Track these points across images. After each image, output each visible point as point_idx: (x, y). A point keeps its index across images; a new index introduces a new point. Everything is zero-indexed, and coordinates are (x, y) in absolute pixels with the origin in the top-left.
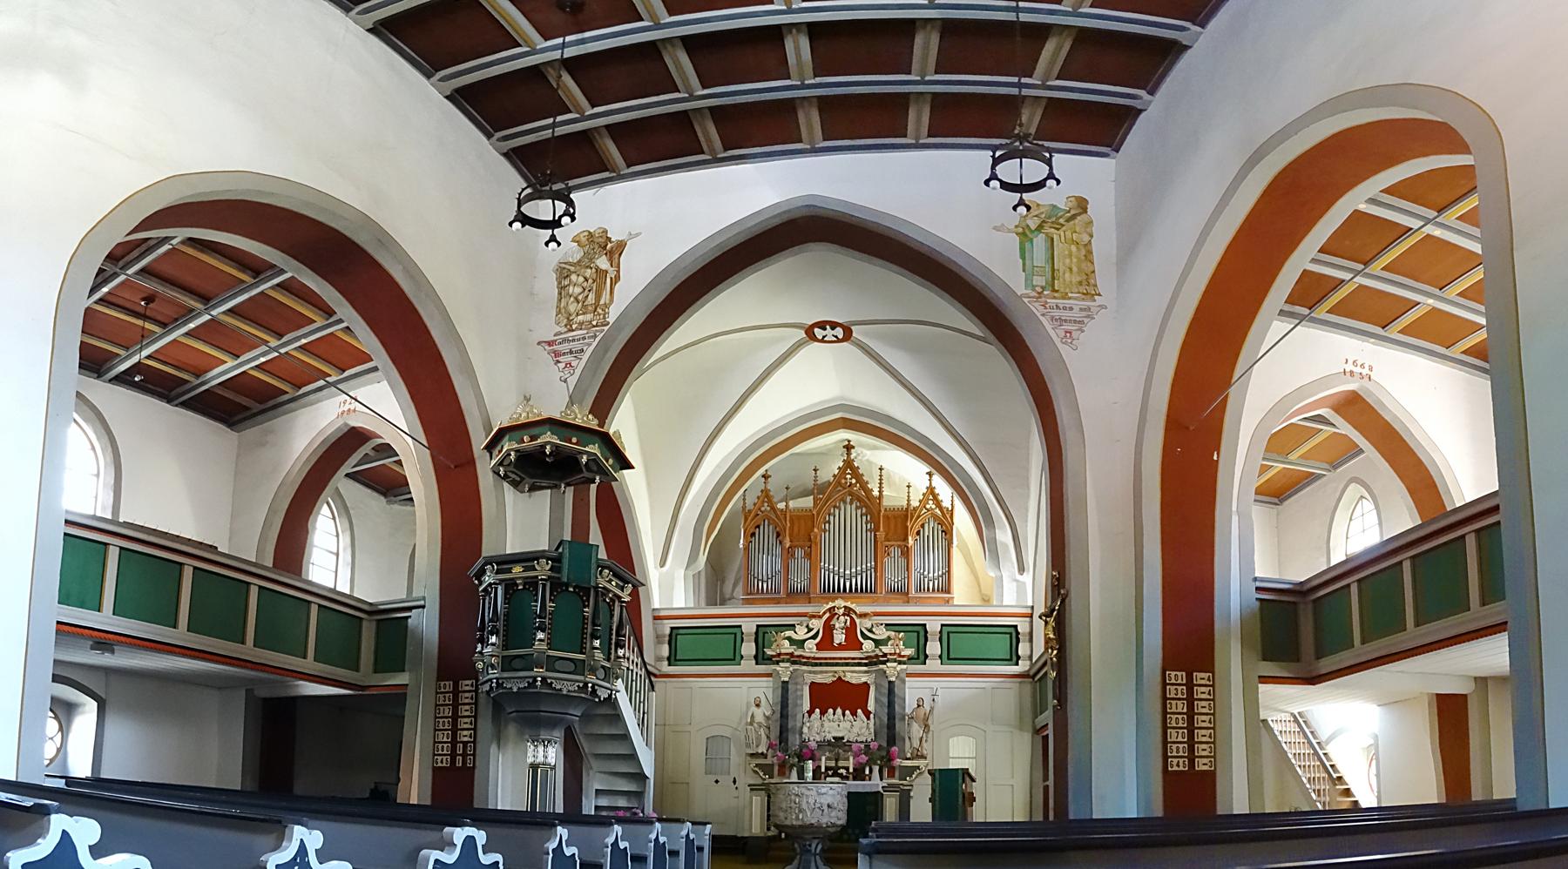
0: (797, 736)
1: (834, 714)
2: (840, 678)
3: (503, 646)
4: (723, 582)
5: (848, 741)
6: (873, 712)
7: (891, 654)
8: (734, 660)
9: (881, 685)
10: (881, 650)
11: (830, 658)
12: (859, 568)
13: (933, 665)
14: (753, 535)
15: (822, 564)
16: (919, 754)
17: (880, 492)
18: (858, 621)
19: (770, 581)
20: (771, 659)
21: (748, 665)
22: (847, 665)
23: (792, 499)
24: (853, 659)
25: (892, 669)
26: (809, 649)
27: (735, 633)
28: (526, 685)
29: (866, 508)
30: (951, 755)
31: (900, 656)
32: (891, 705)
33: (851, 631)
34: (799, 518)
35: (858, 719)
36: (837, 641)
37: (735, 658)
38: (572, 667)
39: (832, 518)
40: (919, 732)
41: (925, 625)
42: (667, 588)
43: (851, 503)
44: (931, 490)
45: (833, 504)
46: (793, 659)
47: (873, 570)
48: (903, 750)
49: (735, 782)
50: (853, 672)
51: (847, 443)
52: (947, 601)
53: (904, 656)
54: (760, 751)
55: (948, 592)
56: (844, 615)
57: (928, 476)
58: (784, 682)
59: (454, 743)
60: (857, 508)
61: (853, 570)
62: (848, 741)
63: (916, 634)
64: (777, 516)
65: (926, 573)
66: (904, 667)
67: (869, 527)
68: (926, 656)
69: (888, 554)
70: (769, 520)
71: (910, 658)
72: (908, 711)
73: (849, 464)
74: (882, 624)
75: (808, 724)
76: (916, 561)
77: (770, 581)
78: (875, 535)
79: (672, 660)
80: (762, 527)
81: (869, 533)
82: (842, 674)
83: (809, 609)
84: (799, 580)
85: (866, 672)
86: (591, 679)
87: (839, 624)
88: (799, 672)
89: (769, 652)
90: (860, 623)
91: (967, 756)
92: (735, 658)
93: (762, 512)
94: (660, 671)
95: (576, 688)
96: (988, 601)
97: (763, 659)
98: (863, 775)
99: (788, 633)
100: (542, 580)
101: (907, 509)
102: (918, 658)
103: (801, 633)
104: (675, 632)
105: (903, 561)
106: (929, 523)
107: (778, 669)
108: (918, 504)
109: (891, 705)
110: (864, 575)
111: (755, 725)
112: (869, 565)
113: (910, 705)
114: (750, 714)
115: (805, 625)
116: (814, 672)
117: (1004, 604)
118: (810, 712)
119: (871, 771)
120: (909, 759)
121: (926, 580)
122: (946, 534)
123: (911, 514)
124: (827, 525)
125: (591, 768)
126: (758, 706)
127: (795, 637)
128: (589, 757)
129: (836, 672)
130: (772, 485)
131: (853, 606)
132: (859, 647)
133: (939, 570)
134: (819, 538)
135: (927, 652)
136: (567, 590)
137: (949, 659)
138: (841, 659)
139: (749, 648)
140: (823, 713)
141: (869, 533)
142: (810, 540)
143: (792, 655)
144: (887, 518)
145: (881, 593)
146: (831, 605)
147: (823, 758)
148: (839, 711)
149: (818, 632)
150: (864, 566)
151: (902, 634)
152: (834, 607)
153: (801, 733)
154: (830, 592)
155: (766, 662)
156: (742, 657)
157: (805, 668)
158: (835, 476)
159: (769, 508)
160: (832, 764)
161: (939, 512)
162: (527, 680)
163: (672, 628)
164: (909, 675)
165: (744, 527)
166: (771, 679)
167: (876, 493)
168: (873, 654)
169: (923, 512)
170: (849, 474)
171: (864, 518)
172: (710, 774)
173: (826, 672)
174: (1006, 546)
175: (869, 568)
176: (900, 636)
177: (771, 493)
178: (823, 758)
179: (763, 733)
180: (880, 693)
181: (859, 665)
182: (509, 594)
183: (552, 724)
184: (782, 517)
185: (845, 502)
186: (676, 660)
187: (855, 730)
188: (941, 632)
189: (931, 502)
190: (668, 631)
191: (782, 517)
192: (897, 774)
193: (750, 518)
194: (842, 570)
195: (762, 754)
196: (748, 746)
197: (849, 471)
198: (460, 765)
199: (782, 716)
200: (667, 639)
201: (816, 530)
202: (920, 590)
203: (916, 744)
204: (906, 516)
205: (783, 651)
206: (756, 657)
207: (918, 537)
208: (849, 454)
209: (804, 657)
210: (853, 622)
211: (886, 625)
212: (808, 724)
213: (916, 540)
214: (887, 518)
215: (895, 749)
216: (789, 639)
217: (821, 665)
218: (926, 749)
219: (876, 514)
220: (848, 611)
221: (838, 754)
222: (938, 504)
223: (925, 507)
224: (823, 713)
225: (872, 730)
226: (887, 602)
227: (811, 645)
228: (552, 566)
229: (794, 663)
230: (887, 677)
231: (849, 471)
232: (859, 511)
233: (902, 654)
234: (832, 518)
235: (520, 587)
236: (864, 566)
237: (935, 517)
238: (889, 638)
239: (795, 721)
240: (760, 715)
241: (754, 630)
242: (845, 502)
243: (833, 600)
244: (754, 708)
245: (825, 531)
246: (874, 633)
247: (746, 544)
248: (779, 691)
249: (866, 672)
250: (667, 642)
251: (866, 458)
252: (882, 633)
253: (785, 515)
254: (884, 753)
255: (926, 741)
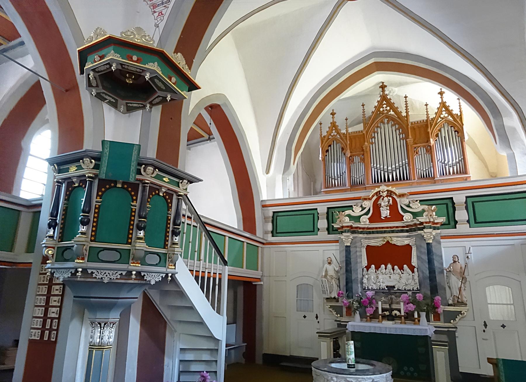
0: (359, 285)
1: (386, 269)
2: (388, 242)
3: (60, 237)
4: (315, 182)
5: (398, 289)
6: (416, 266)
7: (426, 223)
8: (314, 231)
9: (421, 246)
10: (418, 220)
11: (380, 228)
12: (397, 165)
13: (463, 228)
14: (327, 151)
15: (372, 165)
16: (460, 300)
17: (406, 112)
18: (398, 200)
19: (339, 179)
20: (337, 230)
21: (323, 235)
22: (393, 232)
23: (350, 127)
24: (397, 227)
25: (429, 234)
26: (364, 222)
27: (313, 214)
28: (69, 276)
29: (398, 124)
30: (489, 302)
31: (434, 223)
32: (430, 262)
33: (393, 207)
34: (355, 137)
35: (405, 272)
36: (383, 215)
37: (314, 230)
38: (117, 256)
39: (376, 134)
40: (458, 284)
41: (452, 198)
42: (271, 186)
43: (388, 123)
44: (443, 104)
45: (376, 125)
46: (353, 230)
47: (407, 165)
48: (444, 298)
49: (317, 317)
50: (397, 237)
51: (381, 84)
52: (466, 179)
53: (437, 223)
54: (333, 297)
55: (466, 173)
56: (387, 196)
57: (440, 96)
58: (347, 246)
59: (45, 318)
60: (392, 126)
61: (394, 166)
62: (398, 289)
63: (445, 206)
64: (341, 138)
65: (446, 162)
66: (439, 231)
67: (401, 137)
68: (456, 222)
69: (417, 153)
70: (336, 141)
71: (443, 224)
72: (445, 266)
73: (384, 98)
74: (417, 201)
75: (367, 276)
76: (438, 156)
77: (339, 179)
78: (406, 141)
79: (274, 233)
80: (332, 146)
81: (402, 141)
82: (389, 239)
83: (362, 194)
84: (358, 176)
85: (408, 237)
86: (135, 267)
87: (384, 203)
88: (357, 238)
89: (336, 226)
90: (400, 201)
91: (505, 303)
92: (314, 230)
93: (332, 136)
94: (266, 240)
95: (119, 277)
96: (496, 176)
97: (333, 230)
98: (413, 318)
99: (347, 212)
100: (89, 177)
101: (427, 120)
102: (449, 224)
103: (357, 211)
104: (276, 214)
105: (428, 156)
106: (444, 127)
107: (342, 237)
108: (434, 116)
109: (430, 262)
110: (401, 169)
111: (328, 277)
112: (404, 162)
113: (446, 262)
114: (324, 269)
115: (360, 205)
116: (369, 238)
117: (519, 174)
118: (368, 267)
119: (419, 316)
120: (449, 305)
121: (447, 167)
122: (458, 133)
123: (430, 123)
124: (373, 140)
125: (176, 331)
126: (330, 263)
127: (353, 214)
128: (172, 322)
129: (384, 238)
130: (340, 121)
131: (393, 189)
132: (401, 218)
133: (456, 159)
134: (368, 148)
135: (456, 219)
136: (115, 186)
137: (476, 222)
138: (387, 228)
139: (322, 224)
140: (377, 268)
141: (402, 141)
142: (363, 150)
143: (351, 227)
144: (413, 129)
145: (415, 180)
146: (377, 190)
147: (380, 303)
148: (389, 266)
149: (369, 209)
150: (401, 163)
151: (434, 206)
152: (380, 191)
153: (362, 283)
154: (378, 181)
155: (334, 232)
156: (319, 229)
157: (361, 235)
158: (375, 107)
159: (336, 134)
160: (387, 306)
161: (451, 118)
162: (71, 270)
163: (274, 212)
164: (443, 237)
165: (321, 147)
166: (338, 244)
167: (404, 114)
168: (412, 223)
169: (439, 121)
170: (385, 104)
171: (398, 131)
172: (301, 311)
173: (378, 238)
174: (514, 130)
175: (404, 164)
176: (433, 208)
177: (337, 124)
178: (380, 303)
179: (334, 284)
180: (421, 252)
181: (402, 231)
182: (102, 191)
183: (109, 307)
184: (344, 138)
185: (384, 123)
186: (277, 233)
187: (403, 281)
188: (466, 203)
189: (444, 113)
190: (271, 214)
191: (344, 138)
192: (442, 318)
193: (324, 142)
194: (386, 167)
195: (335, 298)
196: (324, 292)
197: (384, 102)
198: (47, 339)
199: (347, 271)
200: (271, 219)
201: (366, 143)
202: (443, 174)
203: (456, 293)
204: (427, 126)
205: (344, 225)
206: (328, 229)
207: (437, 138)
208: (383, 91)
209: (360, 228)
210: (394, 200)
211: (420, 201)
212: (367, 276)
213: (436, 140)
214: (413, 129)
215: (438, 298)
216: (349, 216)
217: (373, 233)
218: (466, 296)
219: (405, 128)
220: (390, 194)
221: (391, 299)
222: (450, 112)
223: (440, 117)
224: (377, 268)
225: (417, 281)
226: (419, 184)
227: (365, 219)
228: (95, 164)
229: (353, 232)
230: (425, 240)
231: (384, 102)
232: (394, 128)
233: (436, 221)
234: (376, 134)
235: (77, 185)
236: (401, 163)
237: (448, 122)
238: (424, 211)
239: (357, 274)
240: (331, 270)
241: (326, 211)
242: (384, 123)
243: (379, 187)
244: (327, 265)
245: (372, 143)
246: (411, 208)
247: (324, 157)
248: (344, 253)
249: (408, 237)
250: (325, 218)
251: (395, 94)
252: (417, 207)
253: (346, 136)
254: (429, 301)
255: (464, 289)
